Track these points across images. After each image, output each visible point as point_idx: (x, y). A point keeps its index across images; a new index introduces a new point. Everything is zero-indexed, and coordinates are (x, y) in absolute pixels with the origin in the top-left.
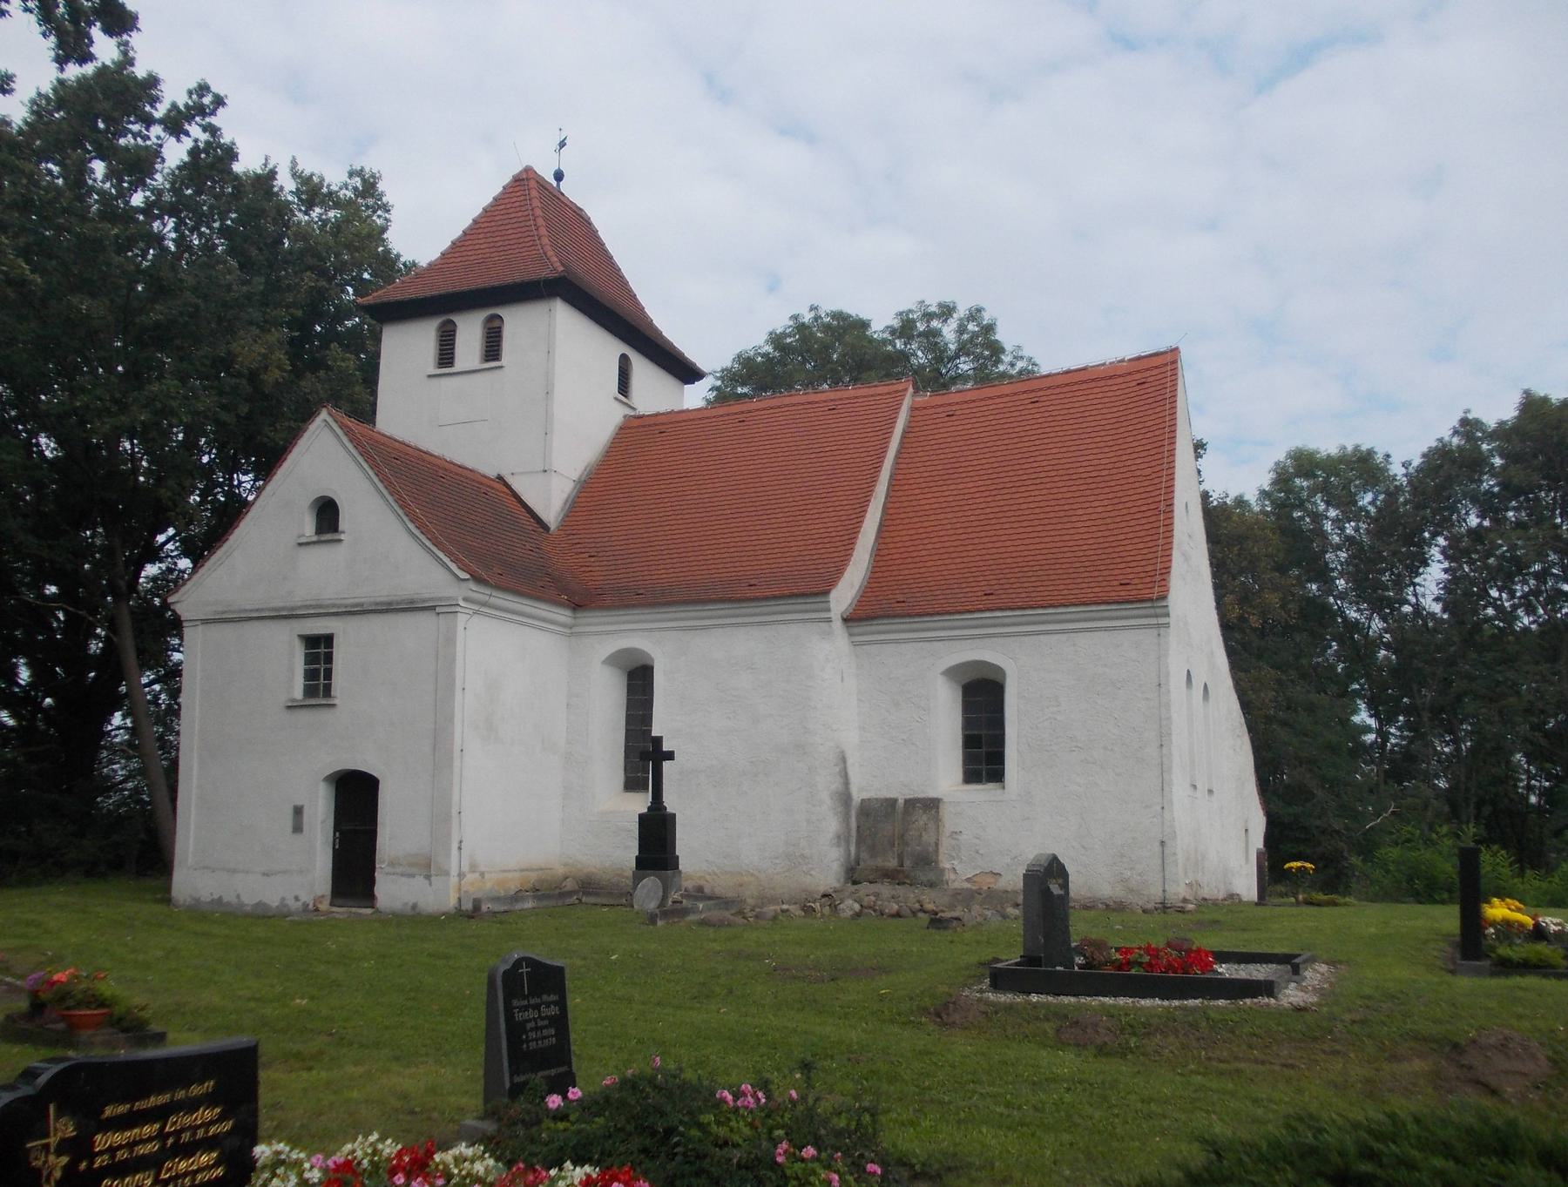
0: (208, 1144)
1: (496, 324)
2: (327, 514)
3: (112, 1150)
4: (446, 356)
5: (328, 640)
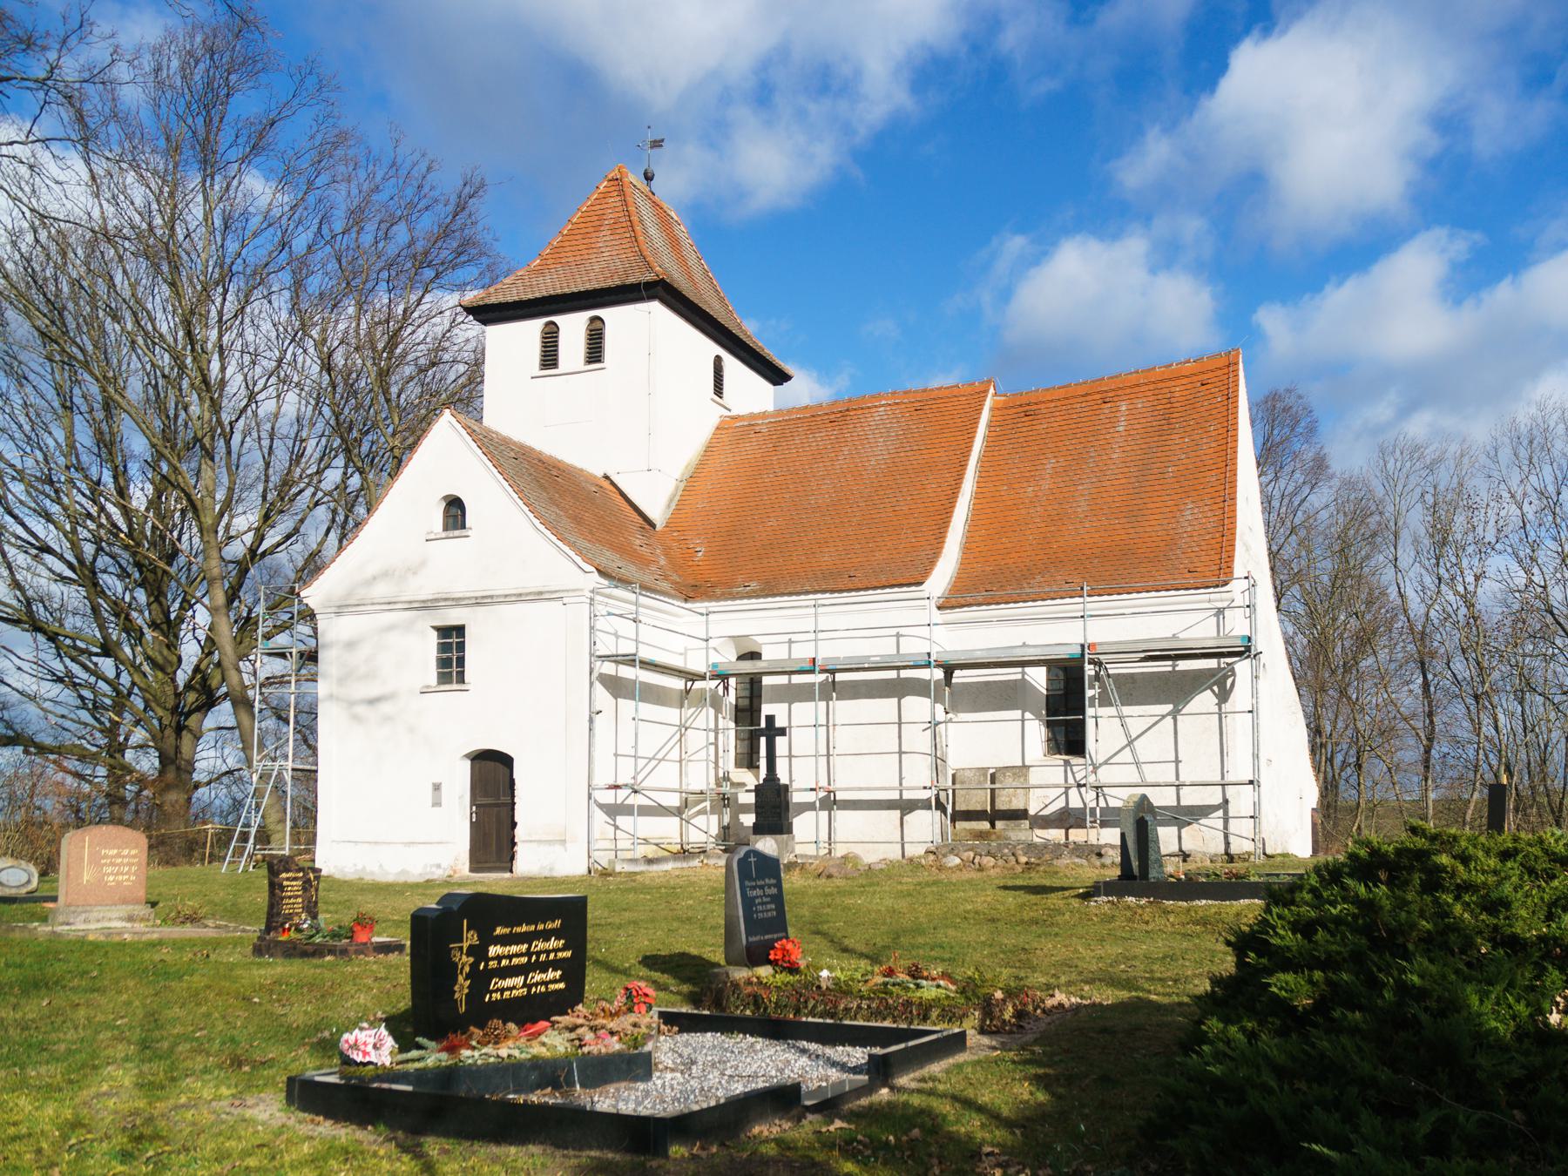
0: (555, 965)
1: (598, 324)
2: (455, 511)
3: (499, 958)
4: (549, 358)
5: (460, 630)
